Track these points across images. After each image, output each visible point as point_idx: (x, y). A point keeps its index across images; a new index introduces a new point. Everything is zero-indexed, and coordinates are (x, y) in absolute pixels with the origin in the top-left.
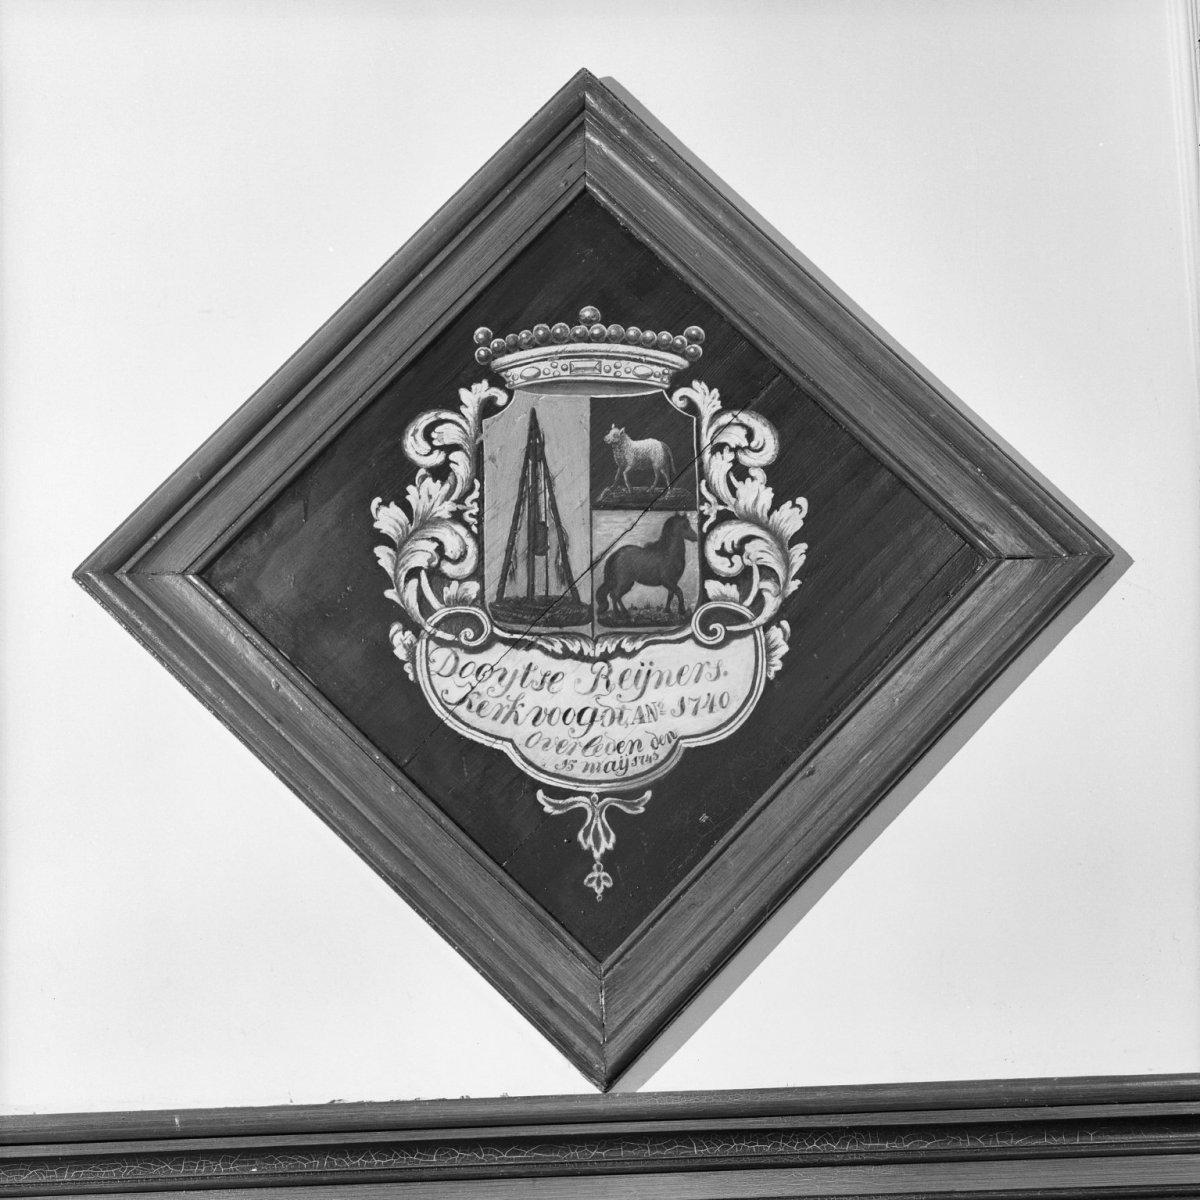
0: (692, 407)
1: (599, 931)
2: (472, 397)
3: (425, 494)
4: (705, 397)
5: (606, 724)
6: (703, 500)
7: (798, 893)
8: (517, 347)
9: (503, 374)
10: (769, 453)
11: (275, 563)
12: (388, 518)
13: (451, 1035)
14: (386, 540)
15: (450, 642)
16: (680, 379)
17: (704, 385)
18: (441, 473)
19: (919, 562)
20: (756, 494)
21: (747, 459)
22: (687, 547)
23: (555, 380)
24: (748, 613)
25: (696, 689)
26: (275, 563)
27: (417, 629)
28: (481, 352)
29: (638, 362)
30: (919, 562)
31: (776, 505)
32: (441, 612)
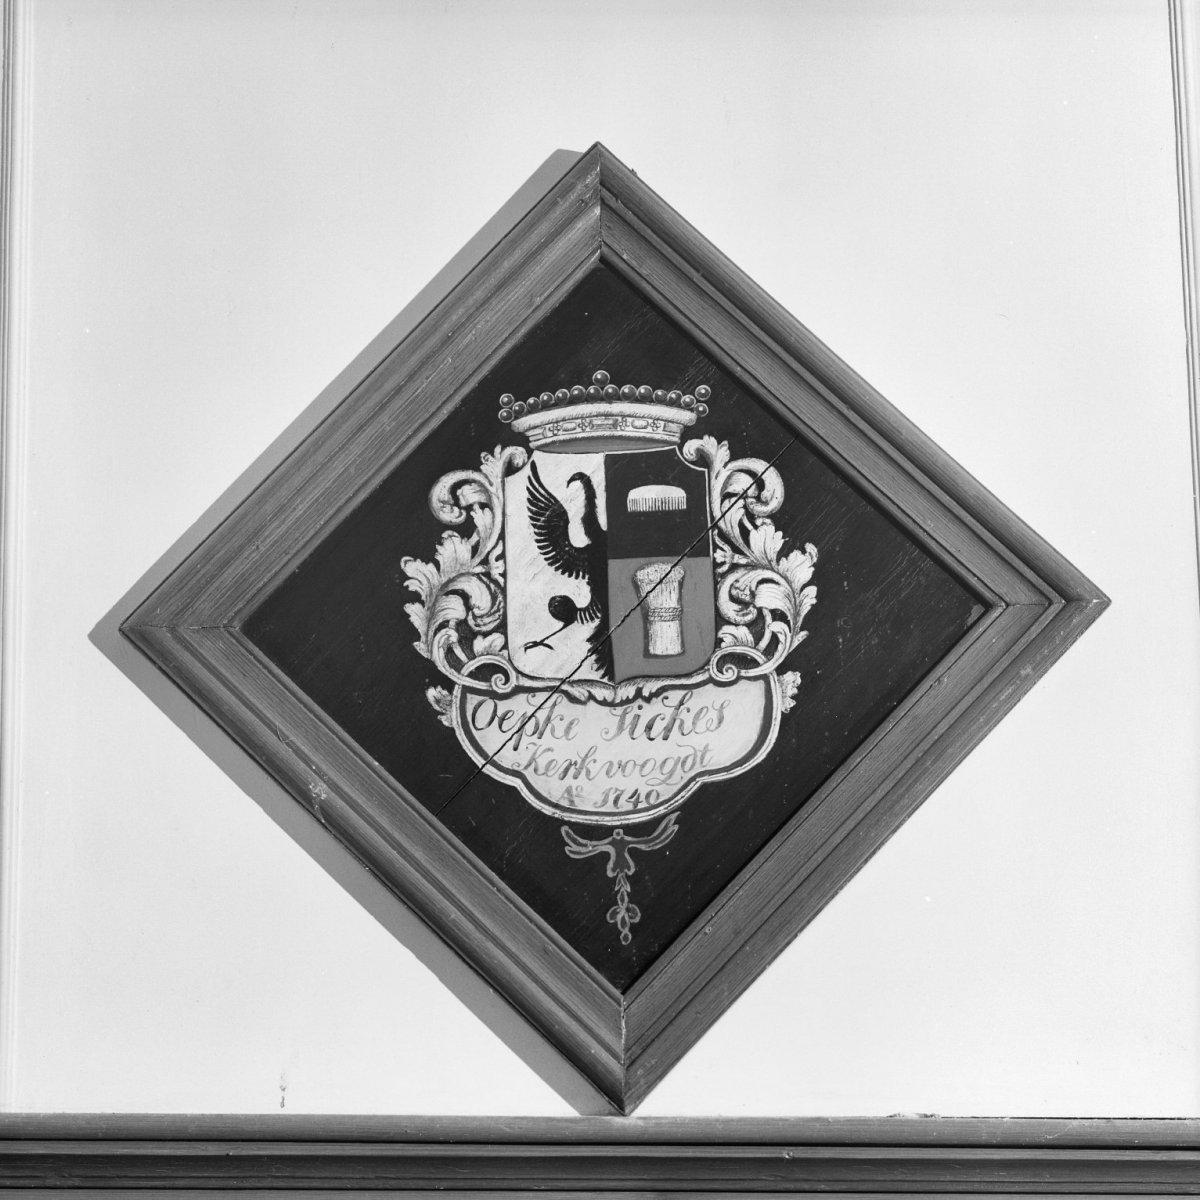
0: (703, 459)
1: (626, 967)
2: (493, 465)
3: (453, 550)
4: (719, 452)
5: (652, 762)
6: (716, 547)
7: (470, 973)
8: (533, 409)
9: (529, 433)
10: (775, 504)
11: (310, 638)
12: (417, 573)
13: (434, 1055)
14: (415, 597)
15: (484, 690)
16: (688, 433)
17: (713, 439)
18: (466, 529)
19: (918, 616)
20: (767, 539)
21: (759, 509)
22: (488, 773)
23: (565, 453)
24: (760, 658)
25: (728, 728)
26: (310, 638)
27: (449, 685)
28: (503, 413)
29: (653, 420)
30: (918, 616)
31: (784, 553)
32: (472, 666)
